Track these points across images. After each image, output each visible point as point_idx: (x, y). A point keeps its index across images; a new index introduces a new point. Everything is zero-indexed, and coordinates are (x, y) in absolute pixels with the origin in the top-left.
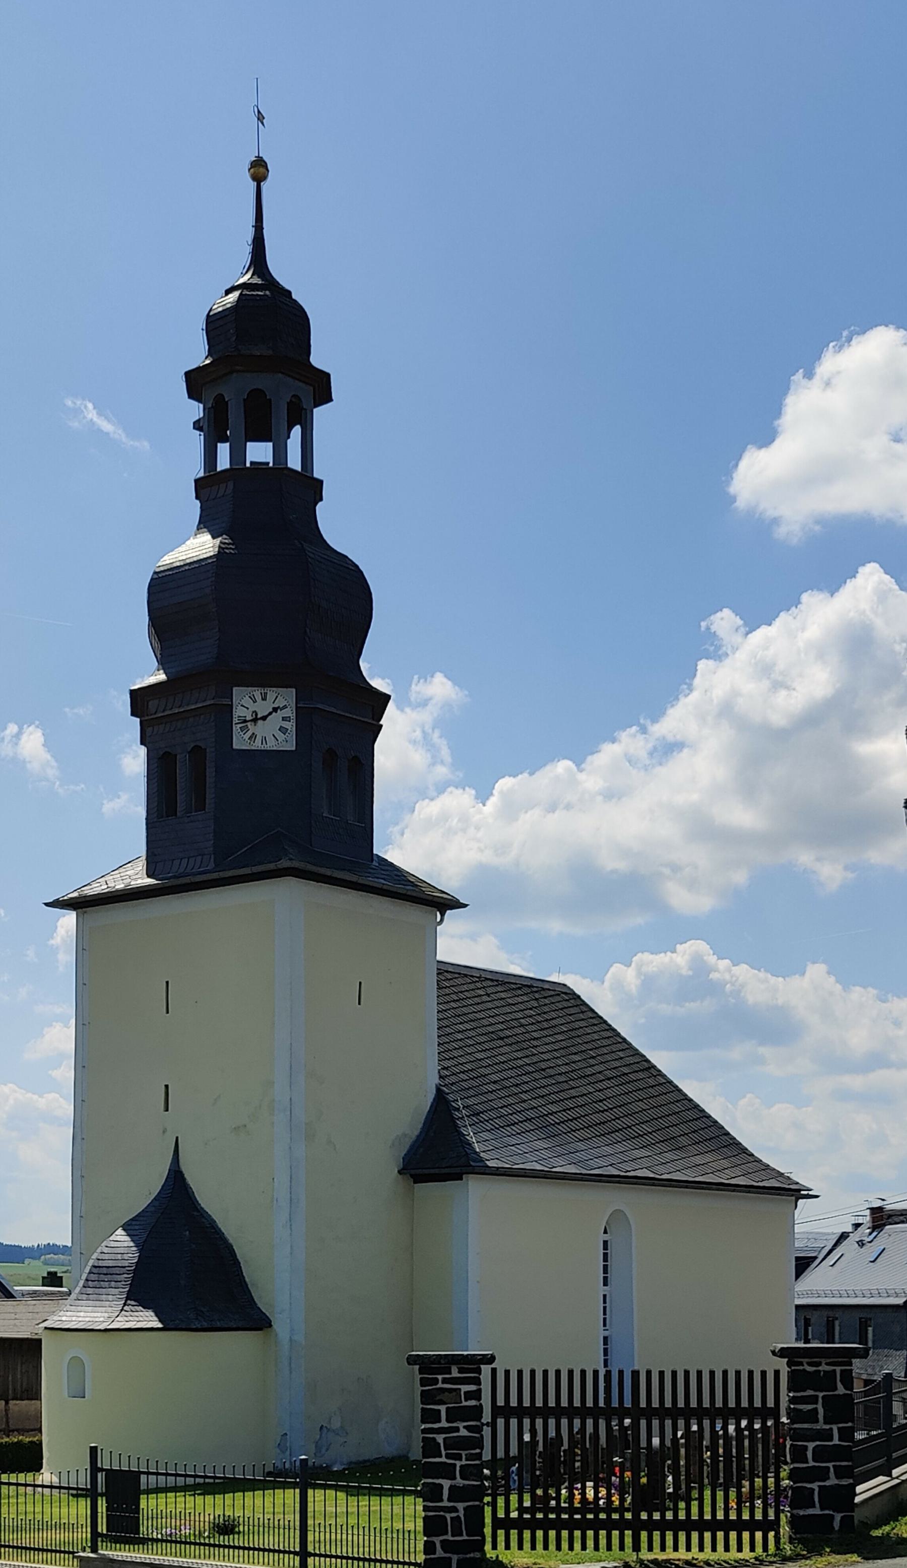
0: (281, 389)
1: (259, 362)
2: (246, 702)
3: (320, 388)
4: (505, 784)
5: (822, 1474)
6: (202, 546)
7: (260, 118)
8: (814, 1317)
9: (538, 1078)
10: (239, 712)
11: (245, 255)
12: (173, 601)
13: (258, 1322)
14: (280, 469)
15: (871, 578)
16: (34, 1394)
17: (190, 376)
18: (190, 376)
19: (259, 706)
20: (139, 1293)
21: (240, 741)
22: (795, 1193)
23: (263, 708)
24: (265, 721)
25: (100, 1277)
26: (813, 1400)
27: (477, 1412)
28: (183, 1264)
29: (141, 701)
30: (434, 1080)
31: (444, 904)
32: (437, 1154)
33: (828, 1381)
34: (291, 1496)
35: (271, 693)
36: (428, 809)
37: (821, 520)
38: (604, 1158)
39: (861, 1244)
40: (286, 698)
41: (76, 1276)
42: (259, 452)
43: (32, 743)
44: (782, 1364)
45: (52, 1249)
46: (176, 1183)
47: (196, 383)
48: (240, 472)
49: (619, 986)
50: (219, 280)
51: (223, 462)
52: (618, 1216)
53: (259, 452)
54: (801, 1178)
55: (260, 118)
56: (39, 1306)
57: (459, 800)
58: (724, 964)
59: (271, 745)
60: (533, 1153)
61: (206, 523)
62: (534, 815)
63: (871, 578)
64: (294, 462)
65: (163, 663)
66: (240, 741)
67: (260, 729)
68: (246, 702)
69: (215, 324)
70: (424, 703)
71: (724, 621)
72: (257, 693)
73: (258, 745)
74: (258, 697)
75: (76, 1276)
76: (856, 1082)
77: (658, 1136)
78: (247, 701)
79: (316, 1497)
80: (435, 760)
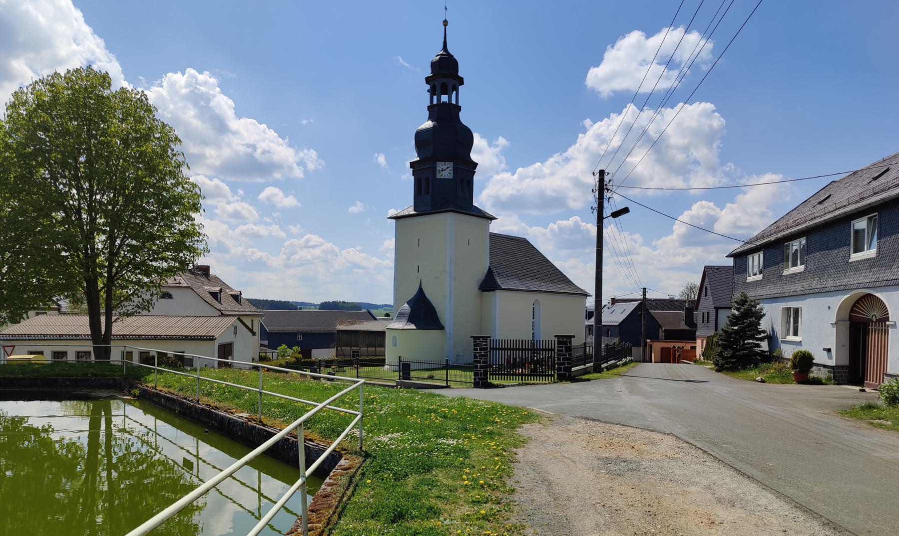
0: (450, 82)
1: (445, 74)
2: (440, 166)
3: (461, 81)
4: (520, 170)
5: (564, 364)
6: (429, 124)
9: (516, 263)
10: (438, 168)
12: (422, 139)
13: (441, 327)
14: (450, 104)
15: (631, 108)
16: (383, 345)
17: (426, 79)
18: (426, 79)
19: (443, 170)
20: (411, 320)
21: (438, 176)
24: (445, 170)
25: (401, 315)
27: (486, 349)
28: (422, 312)
29: (413, 165)
30: (488, 265)
31: (492, 218)
32: (489, 284)
33: (566, 343)
34: (445, 372)
36: (498, 177)
37: (614, 92)
38: (534, 285)
40: (450, 165)
41: (394, 315)
42: (444, 98)
43: (382, 159)
44: (556, 339)
45: (386, 305)
46: (421, 291)
47: (428, 80)
48: (441, 105)
49: (552, 230)
50: (434, 53)
51: (435, 102)
52: (537, 300)
53: (444, 98)
56: (385, 323)
57: (506, 176)
58: (584, 224)
60: (514, 284)
61: (430, 118)
62: (528, 180)
63: (631, 108)
64: (454, 102)
65: (419, 155)
66: (438, 176)
67: (444, 173)
68: (440, 166)
69: (434, 65)
70: (497, 146)
71: (588, 122)
75: (394, 315)
76: (621, 259)
79: (450, 372)
80: (501, 162)
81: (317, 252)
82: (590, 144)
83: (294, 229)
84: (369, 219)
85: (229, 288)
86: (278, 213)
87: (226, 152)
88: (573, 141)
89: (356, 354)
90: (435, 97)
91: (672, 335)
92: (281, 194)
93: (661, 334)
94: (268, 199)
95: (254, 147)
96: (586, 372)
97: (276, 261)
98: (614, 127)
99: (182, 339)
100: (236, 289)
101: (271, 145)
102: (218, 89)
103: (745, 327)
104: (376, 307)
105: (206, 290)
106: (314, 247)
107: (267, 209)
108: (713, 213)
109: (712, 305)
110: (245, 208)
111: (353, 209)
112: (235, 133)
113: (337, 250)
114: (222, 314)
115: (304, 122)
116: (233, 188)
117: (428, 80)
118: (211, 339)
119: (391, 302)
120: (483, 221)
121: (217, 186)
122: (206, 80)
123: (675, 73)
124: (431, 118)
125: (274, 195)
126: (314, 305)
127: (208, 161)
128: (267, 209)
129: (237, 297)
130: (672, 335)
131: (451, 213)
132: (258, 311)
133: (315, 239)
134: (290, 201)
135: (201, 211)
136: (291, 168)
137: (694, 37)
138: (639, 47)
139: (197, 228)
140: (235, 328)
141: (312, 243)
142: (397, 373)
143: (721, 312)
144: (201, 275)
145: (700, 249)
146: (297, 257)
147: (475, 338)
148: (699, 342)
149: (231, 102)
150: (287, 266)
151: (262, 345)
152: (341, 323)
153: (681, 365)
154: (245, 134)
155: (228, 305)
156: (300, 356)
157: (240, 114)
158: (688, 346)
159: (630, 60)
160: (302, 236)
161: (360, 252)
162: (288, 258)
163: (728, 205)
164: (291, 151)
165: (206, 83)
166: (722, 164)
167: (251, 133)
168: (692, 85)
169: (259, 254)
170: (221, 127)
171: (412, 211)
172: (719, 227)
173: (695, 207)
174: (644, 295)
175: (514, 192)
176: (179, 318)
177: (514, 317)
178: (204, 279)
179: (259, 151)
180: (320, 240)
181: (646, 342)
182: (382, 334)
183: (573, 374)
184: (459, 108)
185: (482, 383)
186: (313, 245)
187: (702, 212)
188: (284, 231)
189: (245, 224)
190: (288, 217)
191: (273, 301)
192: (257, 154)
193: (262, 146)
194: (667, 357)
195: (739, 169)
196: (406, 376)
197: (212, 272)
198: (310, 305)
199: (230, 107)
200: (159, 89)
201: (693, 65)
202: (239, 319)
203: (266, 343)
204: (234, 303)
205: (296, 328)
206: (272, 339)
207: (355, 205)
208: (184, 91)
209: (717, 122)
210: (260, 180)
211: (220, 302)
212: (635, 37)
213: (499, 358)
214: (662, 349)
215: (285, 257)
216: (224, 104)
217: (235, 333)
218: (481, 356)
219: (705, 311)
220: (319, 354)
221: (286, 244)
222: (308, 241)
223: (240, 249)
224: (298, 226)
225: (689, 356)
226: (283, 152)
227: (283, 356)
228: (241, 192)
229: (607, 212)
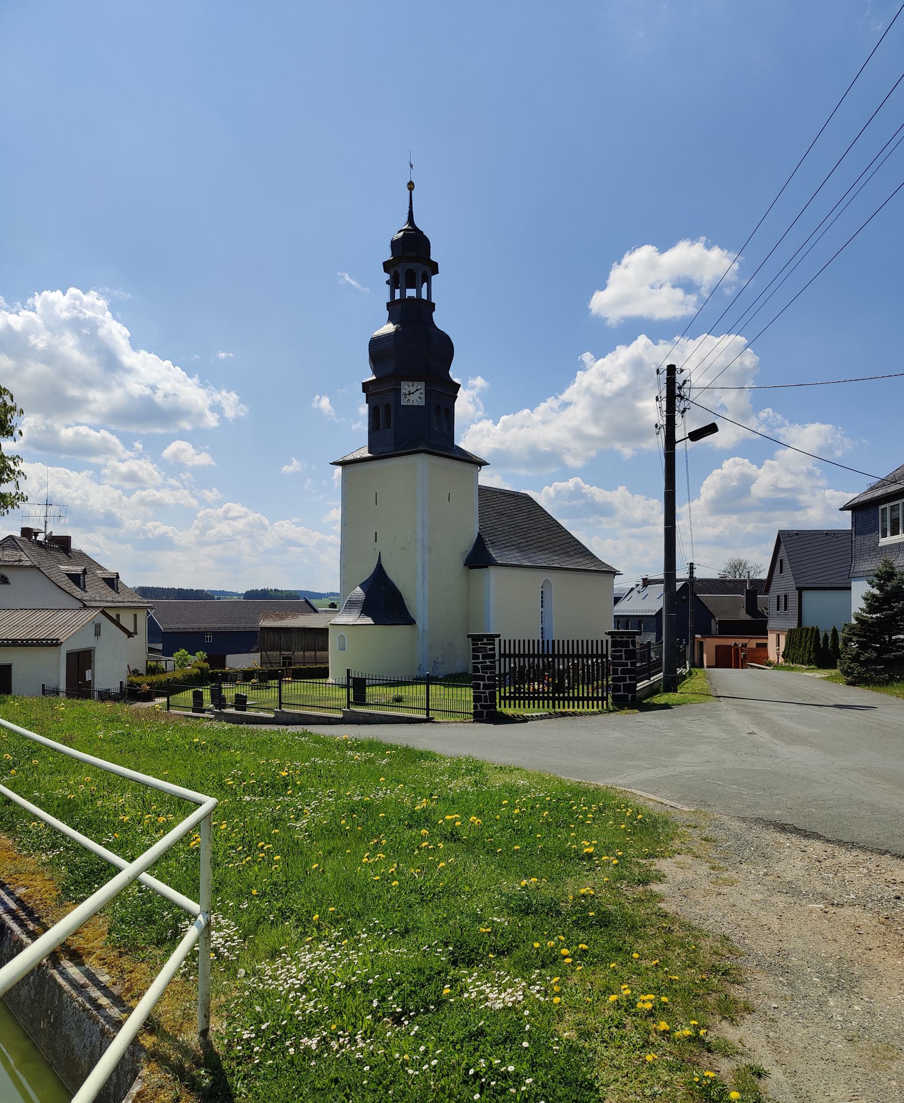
0: (419, 268)
1: (411, 258)
2: (406, 387)
3: (434, 268)
5: (624, 679)
6: (390, 328)
7: (411, 166)
8: (621, 620)
9: (516, 529)
10: (403, 391)
11: (406, 219)
12: (379, 350)
13: (410, 621)
14: (419, 299)
15: (643, 340)
16: (326, 649)
19: (410, 389)
22: (614, 573)
23: (412, 390)
24: (413, 394)
25: (351, 604)
26: (621, 651)
28: (382, 600)
29: (366, 387)
31: (481, 463)
32: (478, 558)
33: (626, 644)
35: (416, 384)
36: (475, 427)
38: (542, 559)
39: (639, 592)
40: (421, 386)
42: (411, 293)
44: (609, 638)
47: (387, 266)
48: (404, 300)
50: (396, 228)
51: (397, 296)
52: (547, 581)
53: (411, 293)
54: (616, 567)
55: (411, 166)
56: (328, 616)
57: (487, 424)
58: (587, 486)
59: (416, 403)
60: (515, 558)
63: (643, 340)
64: (424, 296)
67: (411, 397)
68: (406, 387)
69: (394, 244)
70: (473, 388)
71: (587, 357)
72: (410, 384)
73: (410, 403)
74: (410, 384)
75: (341, 605)
76: (637, 531)
77: (562, 552)
78: (406, 387)
80: (478, 409)
81: (240, 524)
82: (591, 384)
83: (211, 495)
84: (309, 480)
85: (101, 568)
86: (189, 475)
87: (118, 395)
88: (571, 378)
89: (288, 661)
90: (397, 292)
91: (729, 628)
92: (192, 451)
93: (714, 627)
94: (175, 456)
95: (154, 388)
96: (653, 691)
97: (186, 537)
98: (621, 361)
99: (8, 645)
100: (111, 568)
101: (177, 385)
102: (109, 314)
103: (896, 614)
104: (319, 596)
105: (61, 571)
106: (234, 518)
107: (173, 468)
108: (749, 471)
109: (792, 584)
110: (145, 467)
111: (286, 469)
112: (128, 370)
113: (266, 522)
114: (85, 606)
115: (222, 355)
116: (128, 442)
117: (387, 266)
118: (55, 644)
119: (337, 590)
120: (469, 467)
121: (104, 439)
122: (93, 304)
123: (693, 298)
124: (391, 319)
125: (185, 450)
126: (236, 594)
127: (93, 407)
128: (173, 468)
129: (112, 582)
130: (729, 628)
131: (423, 455)
132: (145, 602)
133: (236, 509)
134: (204, 459)
135: (16, 433)
136: (202, 415)
137: (716, 254)
138: (652, 265)
139: (11, 463)
140: (98, 627)
141: (231, 514)
142: (345, 691)
143: (806, 595)
144: (57, 550)
145: (735, 517)
146: (213, 532)
147: (475, 638)
148: (772, 638)
149: (125, 332)
150: (200, 544)
151: (151, 650)
152: (266, 617)
153: (749, 670)
154: (142, 370)
155: (97, 593)
156: (207, 665)
157: (135, 345)
158: (752, 643)
159: (642, 280)
160: (219, 503)
161: (297, 525)
162: (203, 533)
163: (768, 462)
164: (202, 392)
165: (92, 306)
166: (756, 410)
167: (151, 372)
168: (714, 312)
169: (163, 529)
170: (111, 362)
171: (365, 453)
172: (759, 490)
173: (726, 464)
174: (692, 573)
175: (497, 446)
176: (30, 613)
177: (514, 606)
178: (61, 556)
179: (160, 394)
180: (245, 509)
181: (694, 638)
182: (324, 632)
183: (637, 695)
184: (432, 307)
185: (487, 714)
186: (238, 516)
187: (736, 471)
188: (195, 497)
189: (144, 489)
190: (202, 479)
191: (181, 591)
192: (159, 398)
193: (166, 386)
194: (727, 659)
195: (779, 417)
196: (360, 699)
197: (75, 545)
198: (233, 594)
199: (124, 337)
200: (32, 314)
201: (716, 289)
202: (103, 612)
203: (160, 646)
204: (107, 592)
205: (204, 625)
206: (167, 640)
207: (290, 464)
208: (65, 315)
209: (750, 359)
210: (160, 431)
211: (84, 589)
212: (646, 252)
213: (503, 666)
214: (718, 648)
215: (197, 532)
216: (116, 332)
217: (97, 634)
218: (485, 668)
219: (782, 593)
220: (237, 662)
221: (199, 515)
222: (227, 511)
223: (138, 523)
224: (215, 490)
225: (759, 657)
226: (191, 393)
227: (182, 666)
228: (138, 446)
229: (679, 434)
